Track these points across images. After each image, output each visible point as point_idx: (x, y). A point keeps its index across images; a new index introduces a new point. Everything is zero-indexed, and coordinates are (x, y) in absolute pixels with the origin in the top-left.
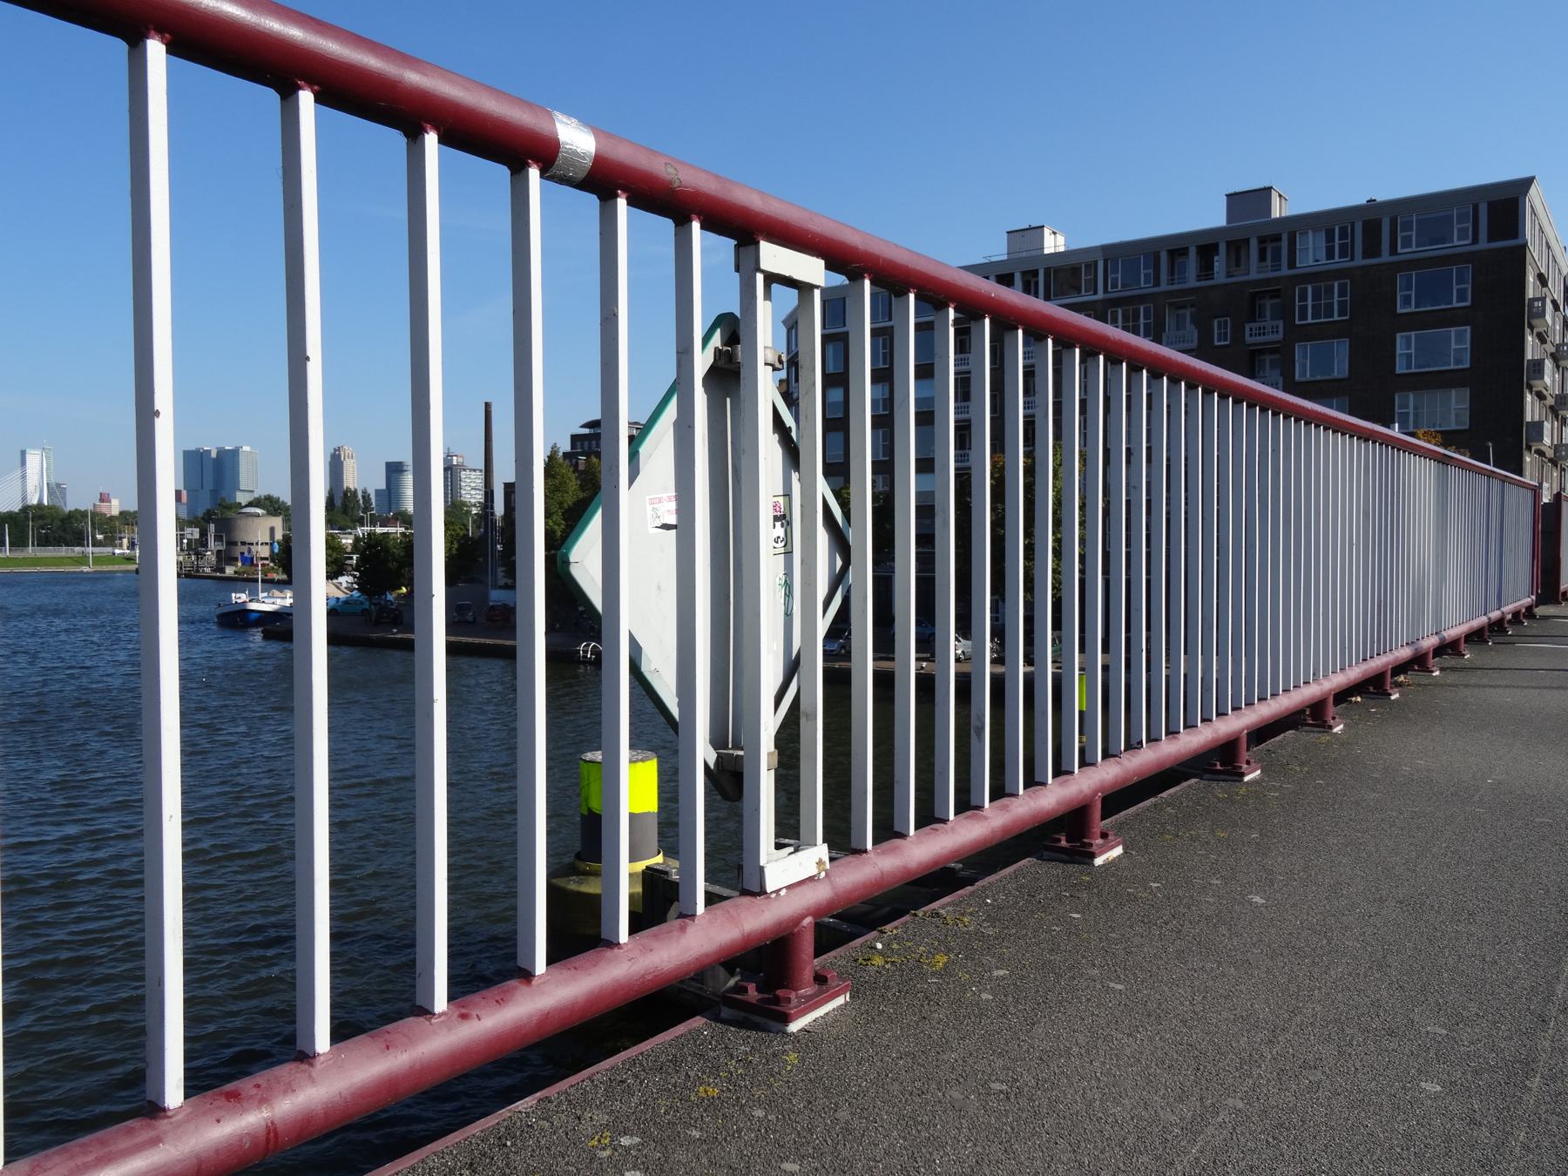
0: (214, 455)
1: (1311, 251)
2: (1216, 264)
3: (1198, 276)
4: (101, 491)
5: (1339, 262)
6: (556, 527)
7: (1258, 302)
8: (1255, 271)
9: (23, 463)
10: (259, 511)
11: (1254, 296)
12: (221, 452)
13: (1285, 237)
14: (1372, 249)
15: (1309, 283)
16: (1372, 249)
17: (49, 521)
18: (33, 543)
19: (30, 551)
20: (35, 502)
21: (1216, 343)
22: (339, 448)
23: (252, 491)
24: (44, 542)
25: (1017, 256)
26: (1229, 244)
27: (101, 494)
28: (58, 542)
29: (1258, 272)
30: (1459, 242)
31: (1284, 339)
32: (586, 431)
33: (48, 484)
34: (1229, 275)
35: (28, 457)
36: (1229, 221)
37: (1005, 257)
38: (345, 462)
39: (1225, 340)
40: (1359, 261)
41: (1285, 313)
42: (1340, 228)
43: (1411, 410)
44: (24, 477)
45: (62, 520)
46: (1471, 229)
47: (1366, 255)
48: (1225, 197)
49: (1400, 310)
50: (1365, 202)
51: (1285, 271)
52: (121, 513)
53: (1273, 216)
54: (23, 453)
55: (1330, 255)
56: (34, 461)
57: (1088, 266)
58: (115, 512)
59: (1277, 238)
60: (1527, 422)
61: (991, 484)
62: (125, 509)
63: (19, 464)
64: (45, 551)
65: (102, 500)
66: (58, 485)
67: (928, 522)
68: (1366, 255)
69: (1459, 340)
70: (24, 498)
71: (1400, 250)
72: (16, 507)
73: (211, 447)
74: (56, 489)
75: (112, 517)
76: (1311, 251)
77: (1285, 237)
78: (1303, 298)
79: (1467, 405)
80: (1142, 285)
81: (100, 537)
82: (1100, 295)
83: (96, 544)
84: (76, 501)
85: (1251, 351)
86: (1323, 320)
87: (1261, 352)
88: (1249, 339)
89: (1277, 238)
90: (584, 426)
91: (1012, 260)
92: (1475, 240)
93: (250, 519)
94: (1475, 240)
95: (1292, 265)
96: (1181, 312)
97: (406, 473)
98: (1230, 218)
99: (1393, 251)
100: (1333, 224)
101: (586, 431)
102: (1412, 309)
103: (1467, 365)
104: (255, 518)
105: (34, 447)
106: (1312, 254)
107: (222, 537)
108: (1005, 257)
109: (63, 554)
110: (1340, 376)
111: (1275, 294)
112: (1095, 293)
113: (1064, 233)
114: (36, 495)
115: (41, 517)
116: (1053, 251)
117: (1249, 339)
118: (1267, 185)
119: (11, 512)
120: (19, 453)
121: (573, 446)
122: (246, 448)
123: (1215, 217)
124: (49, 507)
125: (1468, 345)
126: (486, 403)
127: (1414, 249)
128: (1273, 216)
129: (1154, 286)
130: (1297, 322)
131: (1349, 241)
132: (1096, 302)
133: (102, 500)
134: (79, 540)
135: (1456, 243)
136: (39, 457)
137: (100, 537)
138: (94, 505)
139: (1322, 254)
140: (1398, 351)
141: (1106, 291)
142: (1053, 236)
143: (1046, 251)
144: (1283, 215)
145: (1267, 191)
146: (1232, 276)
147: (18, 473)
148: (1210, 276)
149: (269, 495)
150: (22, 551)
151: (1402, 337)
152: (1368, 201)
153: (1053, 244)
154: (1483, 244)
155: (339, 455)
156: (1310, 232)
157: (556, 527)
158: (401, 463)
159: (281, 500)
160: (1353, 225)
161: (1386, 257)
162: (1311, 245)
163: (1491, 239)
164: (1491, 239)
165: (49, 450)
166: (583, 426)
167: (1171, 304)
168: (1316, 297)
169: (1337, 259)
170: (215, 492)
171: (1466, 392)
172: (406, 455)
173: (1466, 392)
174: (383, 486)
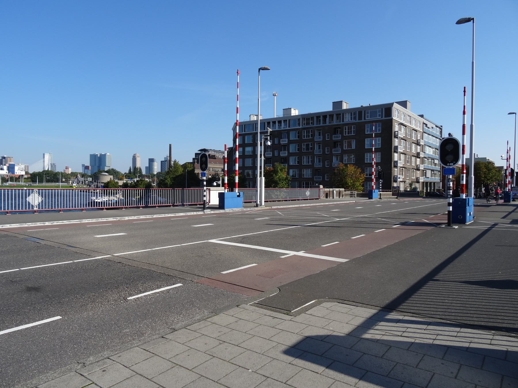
0: (99, 156)
1: (347, 118)
2: (327, 120)
3: (323, 123)
4: (66, 166)
5: (353, 121)
6: (168, 182)
7: (337, 130)
8: (335, 122)
9: (44, 157)
10: (107, 174)
11: (335, 129)
12: (101, 155)
13: (341, 114)
14: (360, 118)
15: (347, 126)
16: (360, 118)
17: (50, 175)
18: (45, 181)
19: (44, 184)
20: (47, 169)
21: (327, 140)
22: (135, 154)
23: (110, 167)
24: (48, 181)
25: (286, 116)
26: (330, 115)
27: (66, 167)
28: (52, 181)
29: (336, 123)
30: (378, 118)
31: (341, 139)
32: (200, 152)
33: (51, 164)
34: (330, 123)
35: (45, 156)
36: (333, 110)
37: (282, 116)
38: (137, 158)
39: (329, 139)
40: (357, 121)
41: (342, 133)
42: (354, 113)
43: (369, 157)
44: (44, 161)
45: (54, 175)
46: (366, 118)
47: (359, 120)
48: (332, 103)
49: (366, 133)
50: (360, 106)
51: (341, 123)
52: (71, 173)
53: (343, 109)
54: (44, 154)
55: (351, 119)
56: (47, 157)
57: (284, 121)
58: (70, 173)
59: (340, 114)
60: (394, 161)
61: (264, 174)
62: (72, 172)
63: (43, 158)
64: (47, 184)
65: (66, 169)
66: (54, 164)
67: (4, 199)
68: (359, 120)
69: (379, 141)
70: (44, 168)
71: (366, 119)
72: (41, 170)
73: (98, 153)
74: (53, 165)
75: (68, 174)
76: (347, 118)
77: (341, 114)
78: (346, 129)
79: (380, 157)
80: (310, 125)
81: (64, 180)
82: (301, 127)
83: (62, 182)
84: (59, 169)
85: (334, 142)
86: (350, 135)
87: (337, 142)
88: (333, 139)
89: (286, 120)
90: (199, 151)
91: (285, 117)
92: (382, 117)
93: (104, 176)
94: (382, 117)
95: (343, 121)
96: (320, 131)
97: (155, 162)
98: (333, 109)
99: (365, 119)
100: (352, 112)
101: (200, 152)
102: (369, 133)
103: (380, 147)
104: (105, 176)
105: (47, 153)
106: (347, 119)
107: (96, 181)
108: (282, 116)
109: (53, 185)
110: (354, 149)
111: (340, 128)
112: (300, 126)
113: (297, 109)
114: (47, 167)
115: (48, 174)
116: (294, 115)
117: (333, 139)
118: (341, 100)
119: (40, 172)
120: (43, 154)
121: (196, 156)
122: (108, 154)
123: (329, 108)
124: (51, 171)
125: (380, 142)
126: (170, 144)
127: (369, 118)
128: (343, 109)
129: (313, 125)
130: (344, 135)
131: (366, 115)
132: (300, 128)
133: (66, 169)
134: (57, 181)
135: (378, 117)
136: (48, 156)
137: (64, 180)
138: (64, 170)
139: (350, 119)
140: (366, 143)
141: (302, 126)
142: (295, 110)
143: (292, 115)
144: (347, 108)
145: (342, 101)
146: (331, 123)
147: (42, 160)
148: (326, 123)
149: (113, 168)
150: (42, 184)
151: (367, 140)
152: (361, 106)
153: (294, 113)
154: (384, 118)
155: (135, 156)
156: (347, 114)
157: (168, 182)
158: (153, 159)
159: (116, 170)
160: (356, 112)
161: (363, 120)
162: (347, 116)
163: (385, 117)
164: (385, 117)
165: (52, 154)
166: (198, 151)
167: (317, 130)
168: (348, 129)
169: (353, 120)
170: (99, 167)
171: (380, 153)
172: (168, 155)
173: (380, 153)
174: (148, 166)
